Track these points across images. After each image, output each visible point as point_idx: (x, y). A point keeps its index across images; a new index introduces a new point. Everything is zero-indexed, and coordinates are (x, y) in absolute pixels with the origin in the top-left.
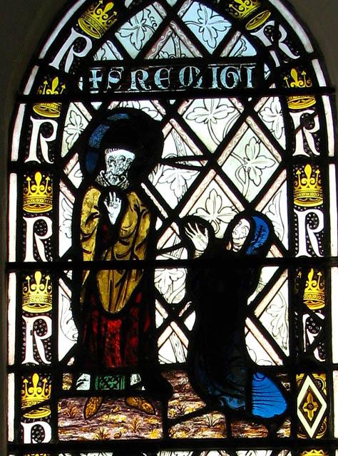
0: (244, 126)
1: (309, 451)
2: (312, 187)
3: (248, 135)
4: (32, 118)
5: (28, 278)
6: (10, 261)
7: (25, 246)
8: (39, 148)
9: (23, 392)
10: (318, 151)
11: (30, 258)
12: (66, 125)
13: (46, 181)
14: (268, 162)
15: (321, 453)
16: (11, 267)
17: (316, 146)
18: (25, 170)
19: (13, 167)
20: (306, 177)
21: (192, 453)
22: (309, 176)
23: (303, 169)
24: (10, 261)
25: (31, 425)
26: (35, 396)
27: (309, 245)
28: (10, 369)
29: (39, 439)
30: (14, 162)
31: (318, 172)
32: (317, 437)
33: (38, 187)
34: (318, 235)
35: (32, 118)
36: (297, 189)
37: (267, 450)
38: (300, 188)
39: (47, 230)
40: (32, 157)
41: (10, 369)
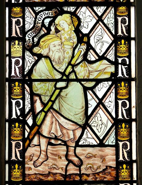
0: (98, 108)
1: (120, 7)
2: (125, 132)
3: (100, 28)
4: (12, 100)
5: (13, 85)
6: (7, 54)
7: (12, 67)
8: (16, 112)
9: (12, 171)
10: (127, 34)
11: (14, 35)
12: (25, 17)
13: (19, 44)
14: (108, 39)
15: (125, 8)
16: (6, 162)
17: (126, 33)
18: (11, 39)
19: (7, 39)
20: (124, 169)
21: (76, 7)
22: (124, 128)
23: (123, 166)
24: (7, 54)
25: (16, 19)
26: (16, 173)
27: (122, 73)
28: (7, 121)
29: (17, 1)
30: (7, 163)
31: (127, 85)
32: (124, 2)
33: (16, 170)
34: (126, 110)
35: (12, 100)
36: (120, 174)
37: (105, 6)
38: (121, 174)
39: (20, 24)
40: (14, 158)
41: (7, 39)
